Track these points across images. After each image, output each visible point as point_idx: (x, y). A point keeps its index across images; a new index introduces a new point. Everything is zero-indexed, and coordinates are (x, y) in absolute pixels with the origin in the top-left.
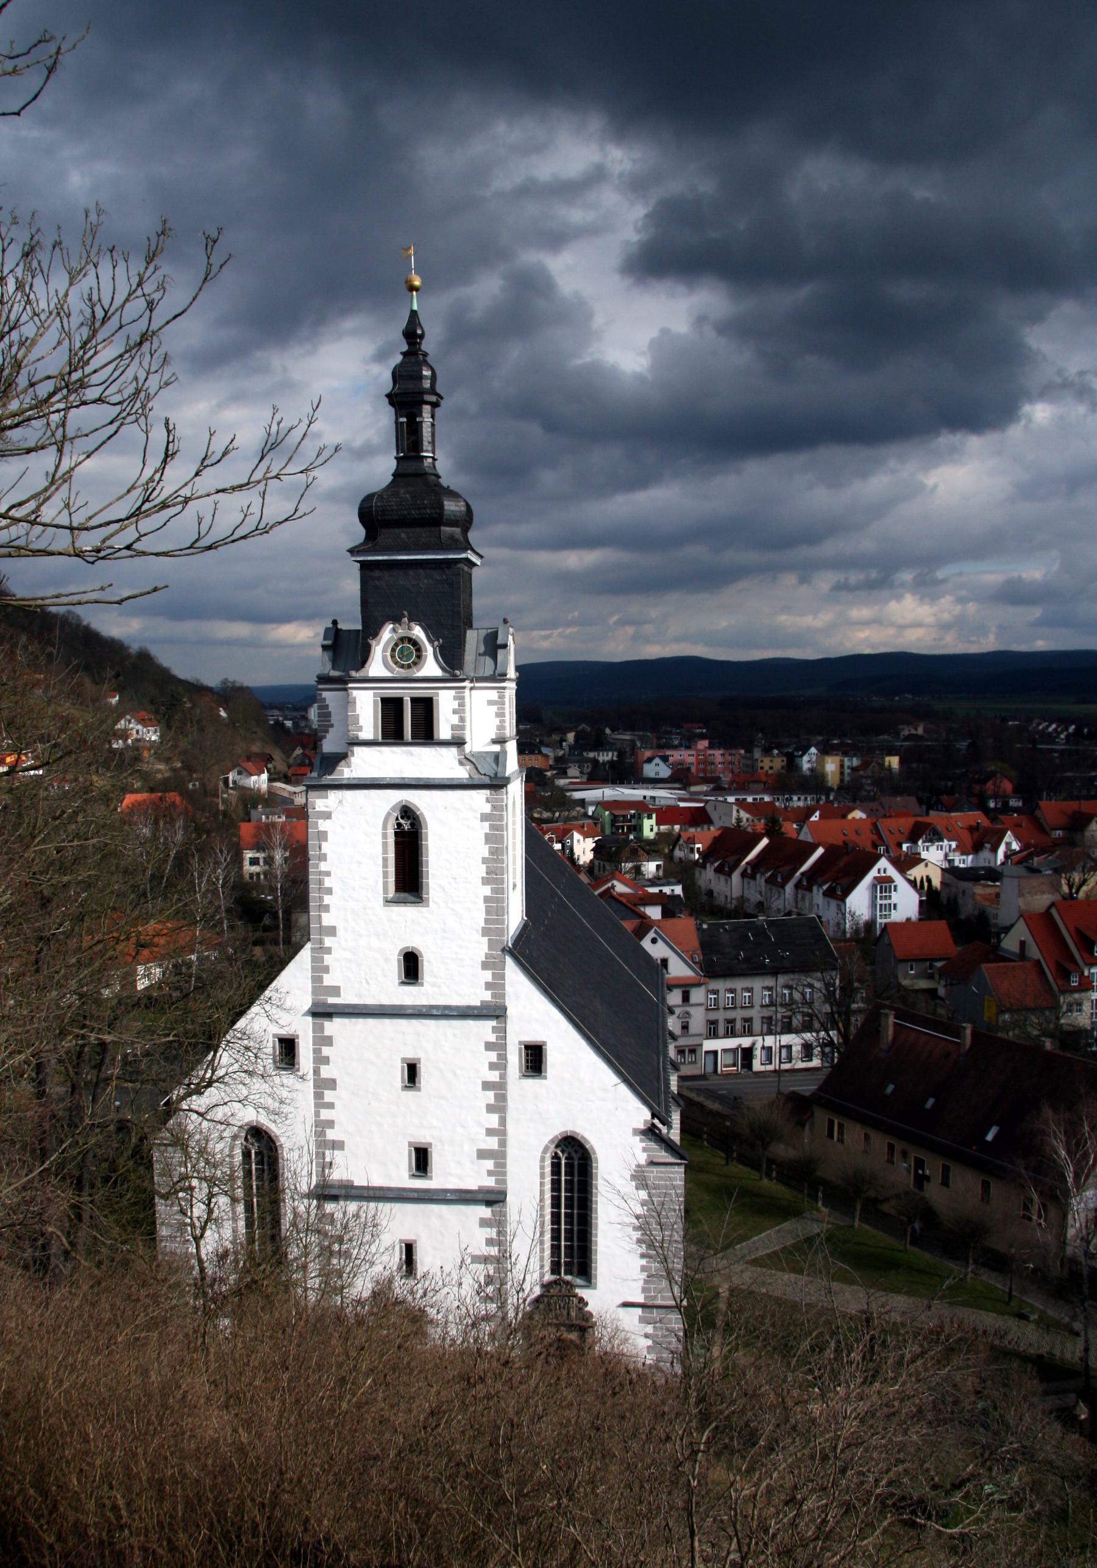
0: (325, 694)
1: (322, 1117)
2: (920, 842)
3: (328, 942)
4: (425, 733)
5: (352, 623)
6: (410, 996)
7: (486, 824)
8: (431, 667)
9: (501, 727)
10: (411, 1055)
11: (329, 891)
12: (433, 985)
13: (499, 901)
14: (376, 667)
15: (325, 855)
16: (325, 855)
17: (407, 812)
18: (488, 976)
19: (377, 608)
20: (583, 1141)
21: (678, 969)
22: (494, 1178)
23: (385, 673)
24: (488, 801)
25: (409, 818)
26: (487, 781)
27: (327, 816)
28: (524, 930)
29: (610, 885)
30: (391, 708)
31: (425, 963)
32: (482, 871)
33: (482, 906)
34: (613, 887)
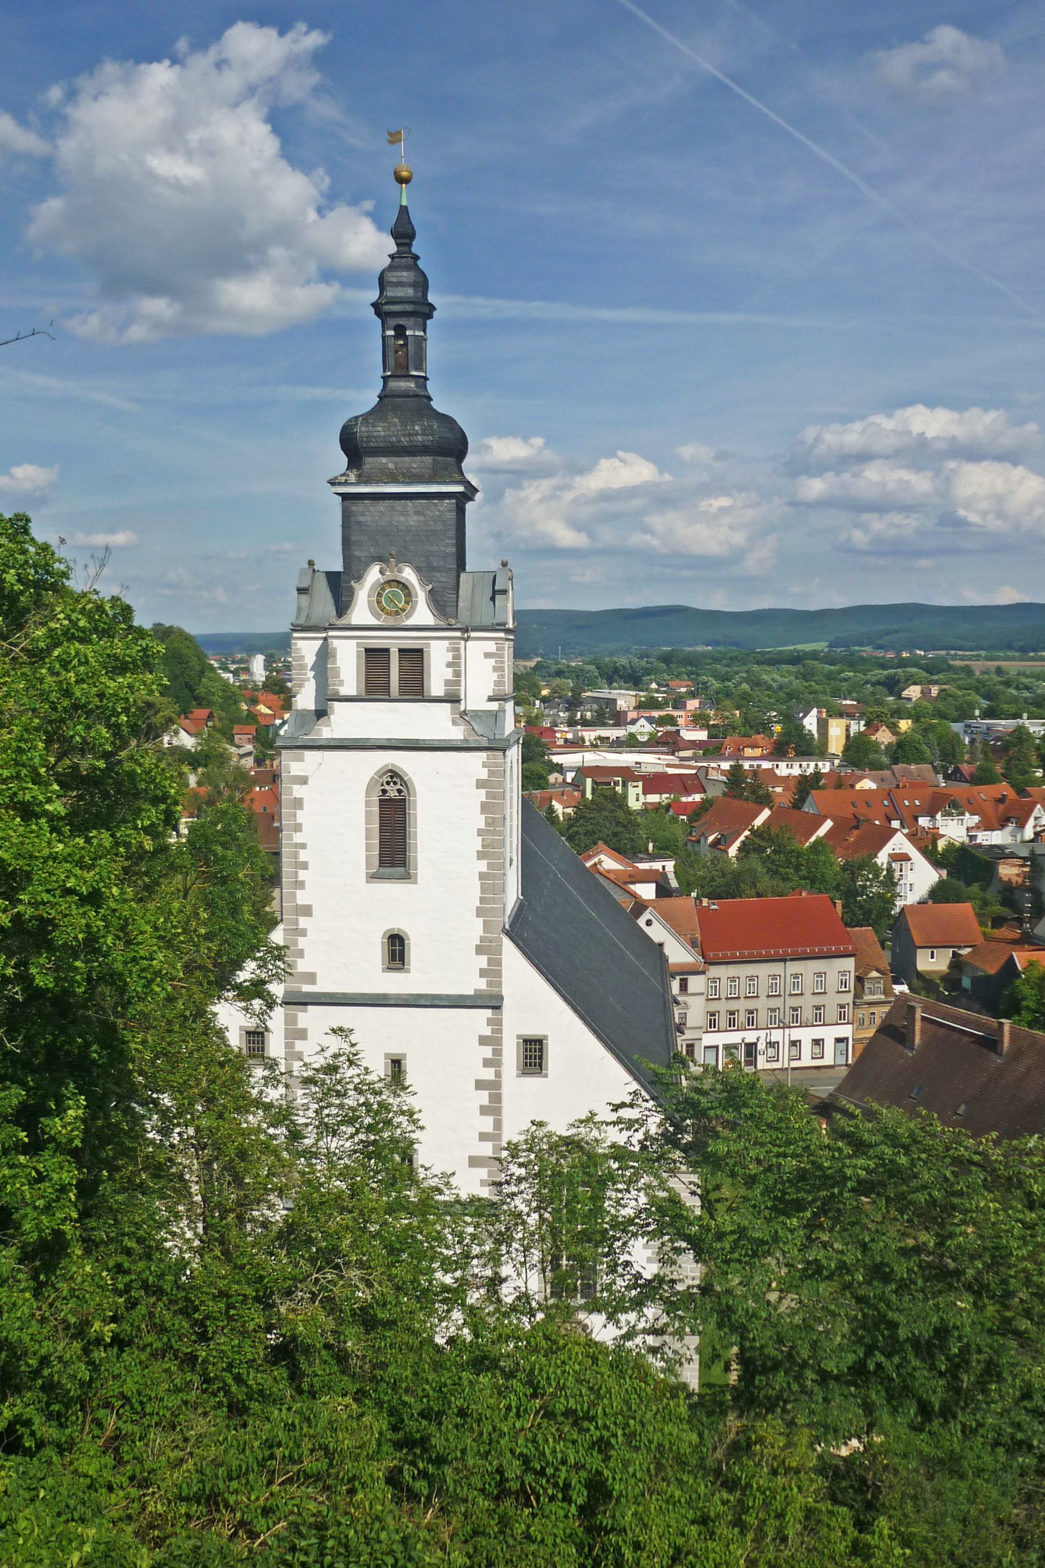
2: (939, 816)
3: (303, 922)
7: (483, 792)
8: (423, 614)
10: (395, 1050)
11: (305, 866)
14: (361, 613)
15: (300, 825)
16: (300, 825)
17: (394, 775)
18: (483, 961)
19: (359, 546)
21: (678, 953)
24: (484, 765)
26: (484, 743)
27: (303, 780)
28: (521, 909)
29: (596, 860)
30: (375, 657)
31: (412, 947)
32: (477, 844)
33: (478, 884)
34: (600, 862)
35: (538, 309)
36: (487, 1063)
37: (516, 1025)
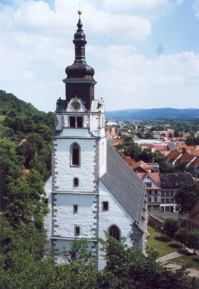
0: (57, 116)
1: (53, 219)
3: (56, 176)
4: (80, 125)
5: (64, 98)
6: (77, 190)
8: (82, 109)
9: (99, 125)
11: (57, 163)
12: (81, 186)
13: (98, 166)
19: (69, 95)
20: (117, 227)
22: (95, 236)
23: (71, 111)
25: (76, 146)
27: (56, 145)
32: (94, 159)
33: (94, 168)
35: (71, 161)
36: (55, 221)
37: (102, 199)
